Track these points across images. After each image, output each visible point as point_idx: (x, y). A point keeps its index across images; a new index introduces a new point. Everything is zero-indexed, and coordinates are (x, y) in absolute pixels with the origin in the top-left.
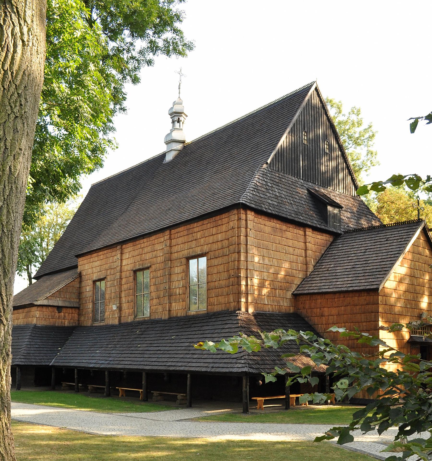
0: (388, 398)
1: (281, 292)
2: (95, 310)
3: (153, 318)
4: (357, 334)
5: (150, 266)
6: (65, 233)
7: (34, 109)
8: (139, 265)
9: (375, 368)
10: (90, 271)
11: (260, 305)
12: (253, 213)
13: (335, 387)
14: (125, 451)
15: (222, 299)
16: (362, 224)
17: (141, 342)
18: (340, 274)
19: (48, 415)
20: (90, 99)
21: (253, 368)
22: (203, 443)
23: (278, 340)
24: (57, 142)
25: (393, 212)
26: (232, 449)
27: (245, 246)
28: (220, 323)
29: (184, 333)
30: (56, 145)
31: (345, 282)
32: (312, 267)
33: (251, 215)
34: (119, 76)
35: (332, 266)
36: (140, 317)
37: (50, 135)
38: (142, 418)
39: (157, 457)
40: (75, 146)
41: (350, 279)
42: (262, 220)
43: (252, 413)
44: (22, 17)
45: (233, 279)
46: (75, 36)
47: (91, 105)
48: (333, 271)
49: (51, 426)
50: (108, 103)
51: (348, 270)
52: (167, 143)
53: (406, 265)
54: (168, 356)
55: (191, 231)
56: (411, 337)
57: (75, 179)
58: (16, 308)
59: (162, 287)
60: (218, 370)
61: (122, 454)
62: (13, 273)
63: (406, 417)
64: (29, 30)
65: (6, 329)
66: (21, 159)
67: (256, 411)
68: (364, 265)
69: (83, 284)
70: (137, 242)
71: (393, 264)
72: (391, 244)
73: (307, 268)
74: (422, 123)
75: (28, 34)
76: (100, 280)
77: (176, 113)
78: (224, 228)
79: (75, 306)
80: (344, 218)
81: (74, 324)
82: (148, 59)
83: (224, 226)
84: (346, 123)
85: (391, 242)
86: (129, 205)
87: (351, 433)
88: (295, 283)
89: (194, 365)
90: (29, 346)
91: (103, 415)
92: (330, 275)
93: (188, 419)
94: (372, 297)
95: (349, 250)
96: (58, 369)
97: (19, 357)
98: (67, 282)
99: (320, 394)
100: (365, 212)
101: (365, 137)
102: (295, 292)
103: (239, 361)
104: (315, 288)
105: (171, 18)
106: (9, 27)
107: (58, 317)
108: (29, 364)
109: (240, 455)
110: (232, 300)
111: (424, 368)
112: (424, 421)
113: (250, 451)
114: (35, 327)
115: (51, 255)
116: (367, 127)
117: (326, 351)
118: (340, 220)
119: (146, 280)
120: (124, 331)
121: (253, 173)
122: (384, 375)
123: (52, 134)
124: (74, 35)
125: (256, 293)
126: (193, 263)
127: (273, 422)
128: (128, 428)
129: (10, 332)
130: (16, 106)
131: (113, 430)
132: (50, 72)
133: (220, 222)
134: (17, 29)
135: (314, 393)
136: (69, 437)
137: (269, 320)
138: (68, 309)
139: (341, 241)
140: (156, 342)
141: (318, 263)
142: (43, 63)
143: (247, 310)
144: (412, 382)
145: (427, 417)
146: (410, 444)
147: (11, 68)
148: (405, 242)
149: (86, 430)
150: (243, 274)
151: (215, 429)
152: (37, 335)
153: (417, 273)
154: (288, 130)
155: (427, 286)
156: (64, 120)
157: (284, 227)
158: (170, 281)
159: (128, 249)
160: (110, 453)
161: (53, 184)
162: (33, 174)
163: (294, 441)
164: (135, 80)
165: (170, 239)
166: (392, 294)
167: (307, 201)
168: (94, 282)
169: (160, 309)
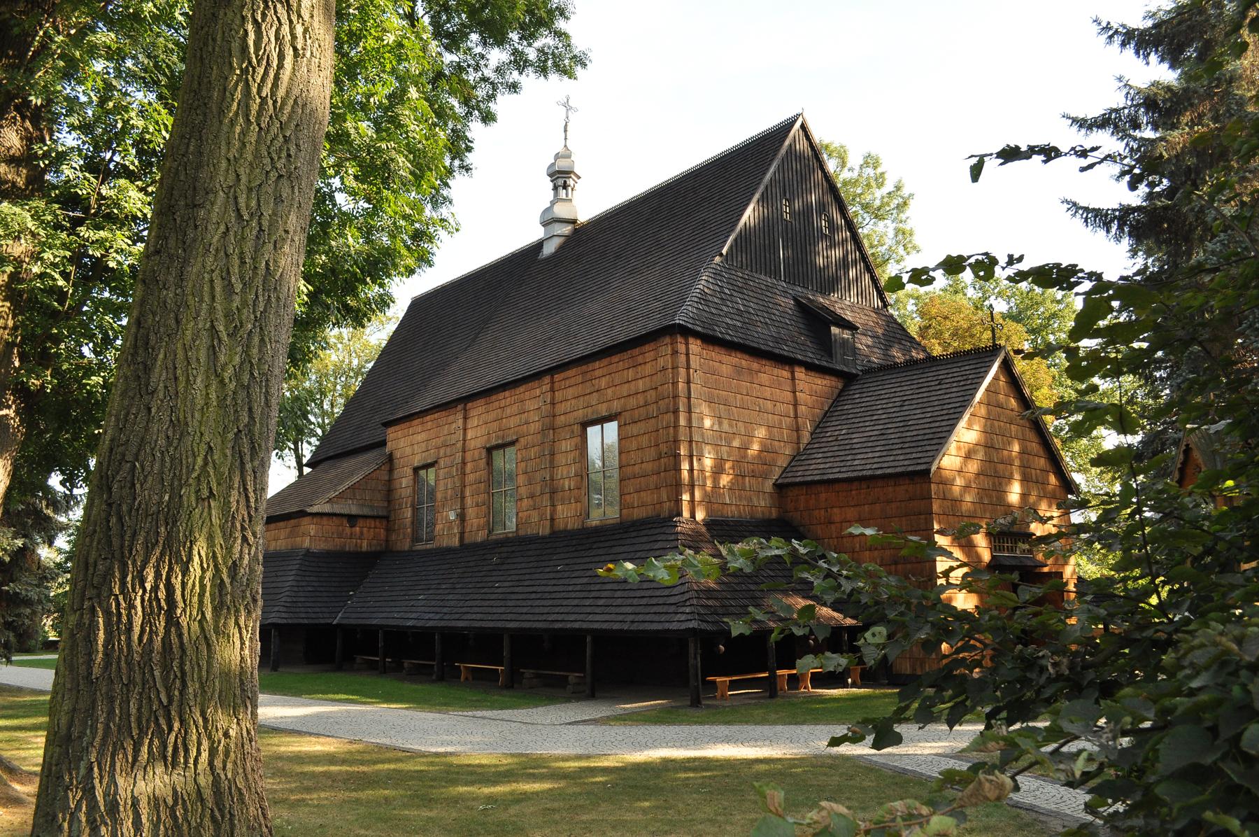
0: (963, 658)
1: (753, 481)
2: (416, 522)
3: (522, 533)
4: (899, 538)
5: (517, 440)
6: (364, 383)
7: (311, 162)
8: (497, 437)
9: (935, 604)
10: (408, 450)
11: (716, 506)
12: (699, 342)
13: (862, 641)
14: (472, 783)
15: (647, 497)
16: (894, 357)
17: (502, 578)
18: (858, 446)
19: (328, 716)
20: (411, 149)
21: (708, 622)
22: (617, 765)
23: (752, 557)
24: (351, 221)
25: (947, 335)
26: (671, 775)
27: (686, 400)
28: (645, 539)
29: (579, 561)
30: (350, 227)
31: (869, 461)
32: (808, 434)
33: (695, 346)
34: (460, 110)
35: (844, 432)
36: (499, 532)
37: (340, 209)
38: (502, 720)
39: (532, 793)
40: (383, 230)
41: (877, 454)
42: (715, 354)
43: (708, 706)
44: (295, 9)
45: (666, 460)
46: (385, 42)
47: (411, 157)
48: (846, 442)
49: (332, 737)
50: (442, 154)
51: (872, 439)
52: (546, 223)
53: (976, 427)
54: (550, 603)
55: (588, 376)
56: (993, 557)
57: (382, 285)
58: (271, 520)
59: (538, 476)
60: (642, 627)
61: (466, 788)
62: (268, 452)
63: (998, 693)
64: (306, 31)
65: (252, 553)
66: (286, 249)
67: (714, 702)
68: (902, 429)
69: (396, 474)
70: (494, 397)
71: (953, 426)
72: (948, 391)
73: (798, 438)
74: (991, 165)
75: (305, 37)
76: (427, 466)
77: (559, 172)
78: (648, 369)
79: (380, 514)
80: (860, 346)
81: (379, 548)
82: (511, 80)
83: (648, 366)
84: (854, 183)
85: (948, 386)
86: (479, 333)
87: (898, 728)
88: (779, 463)
89: (598, 618)
90: (296, 589)
91: (431, 716)
92: (841, 448)
93: (588, 720)
94: (918, 486)
95: (873, 403)
96: (347, 631)
97: (276, 609)
98: (367, 470)
99: (834, 655)
100: (898, 336)
101: (892, 206)
102: (779, 481)
103: (681, 610)
104: (816, 472)
105: (550, 12)
106: (271, 26)
108: (296, 621)
109: (687, 785)
110: (665, 498)
111: (1027, 597)
112: (1033, 702)
113: (705, 777)
114: (308, 553)
115: (339, 423)
116: (892, 189)
117: (841, 575)
118: (855, 351)
119: (510, 466)
120: (469, 559)
121: (698, 273)
122: (952, 616)
123: (344, 209)
124: (383, 40)
125: (709, 483)
126: (593, 432)
127: (747, 723)
128: (478, 738)
129: (261, 558)
130: (279, 158)
131: (450, 743)
132: (342, 102)
133: (640, 359)
134: (286, 29)
135: (823, 654)
136: (367, 757)
137: (733, 533)
138: (368, 521)
139: (857, 387)
140: (527, 577)
141: (818, 427)
142: (330, 87)
143: (693, 515)
144: (1004, 629)
145: (1038, 692)
146: (1013, 735)
147: (273, 93)
148: (974, 386)
149: (400, 743)
150: (683, 451)
151: (640, 738)
152: (311, 569)
153: (998, 441)
154: (757, 196)
155: (1017, 463)
156: (363, 183)
157: (755, 366)
158: (552, 466)
159: (478, 410)
160: (444, 787)
161: (344, 296)
162: (308, 278)
163: (788, 756)
164: (488, 118)
165: (552, 390)
166: (954, 479)
167: (794, 318)
168: (416, 470)
169: (535, 516)
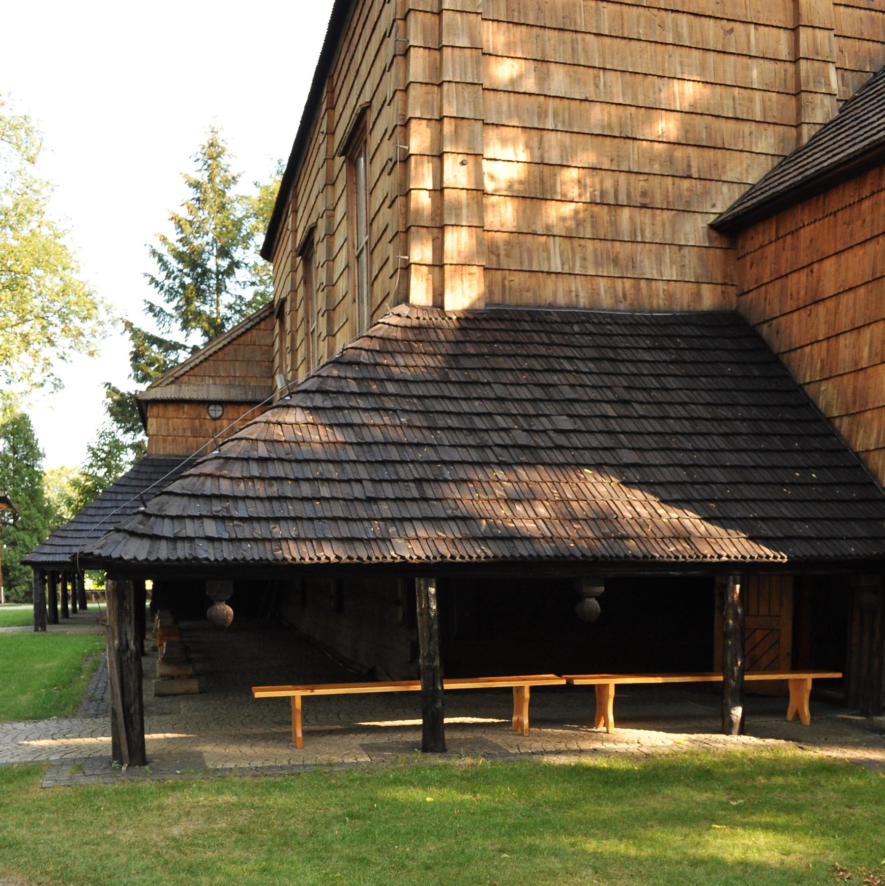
107: (210, 431)
